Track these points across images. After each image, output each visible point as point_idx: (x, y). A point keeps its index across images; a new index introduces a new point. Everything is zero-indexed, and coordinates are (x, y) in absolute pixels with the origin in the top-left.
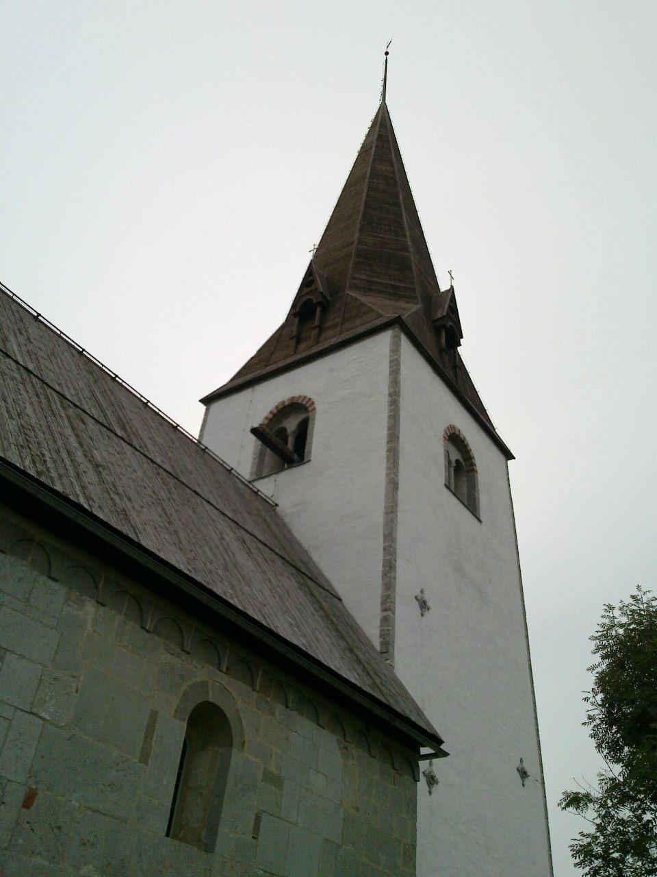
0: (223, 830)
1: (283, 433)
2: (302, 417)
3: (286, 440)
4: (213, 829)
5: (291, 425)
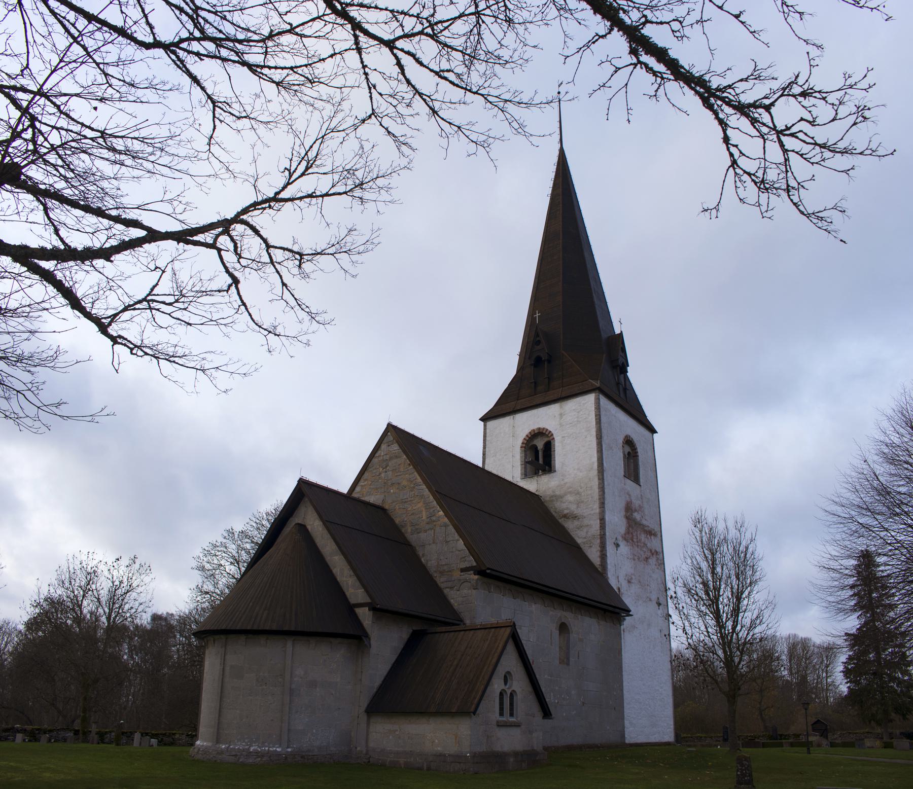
0: (572, 659)
1: (535, 449)
2: (546, 440)
3: (539, 454)
4: (568, 659)
5: (540, 444)
